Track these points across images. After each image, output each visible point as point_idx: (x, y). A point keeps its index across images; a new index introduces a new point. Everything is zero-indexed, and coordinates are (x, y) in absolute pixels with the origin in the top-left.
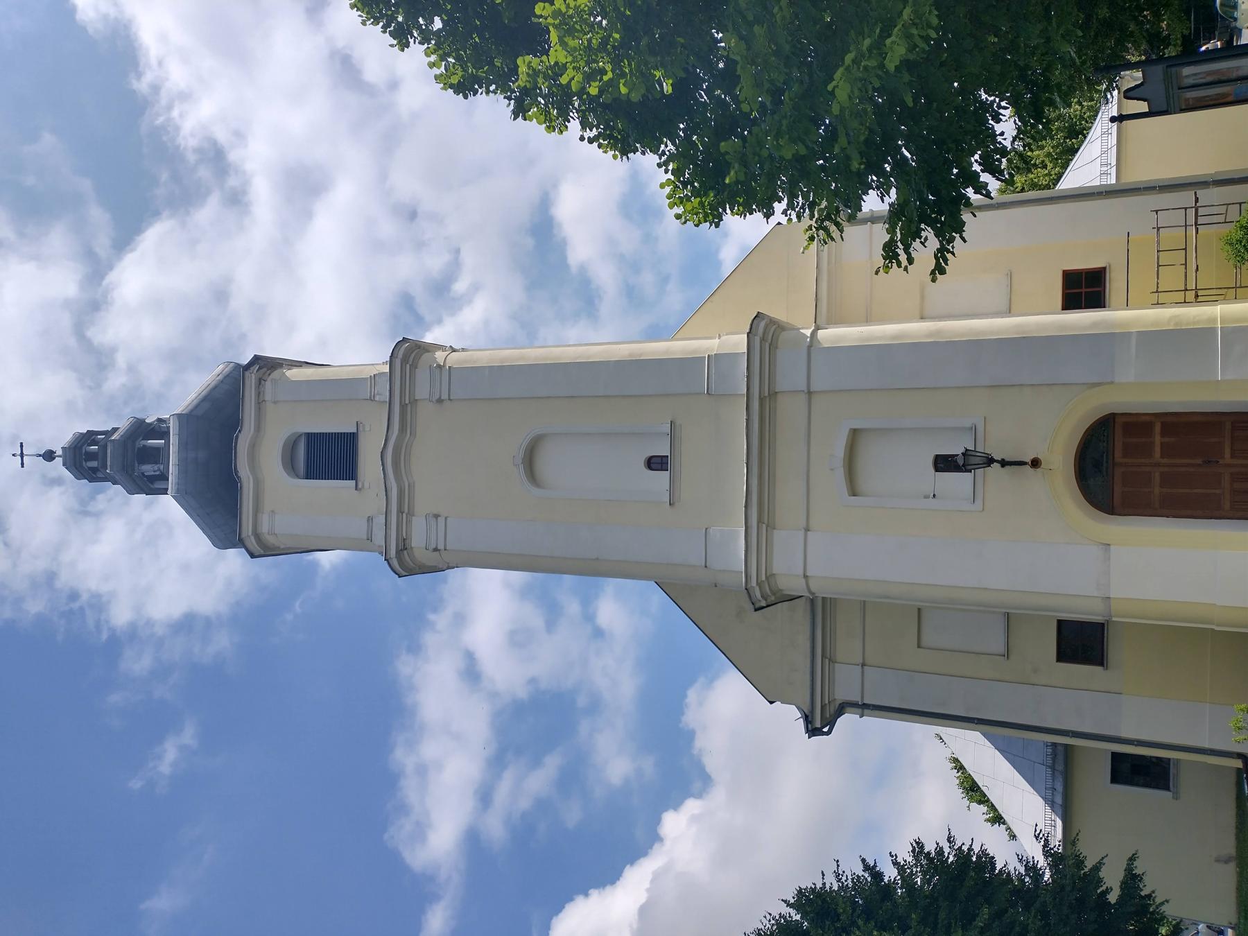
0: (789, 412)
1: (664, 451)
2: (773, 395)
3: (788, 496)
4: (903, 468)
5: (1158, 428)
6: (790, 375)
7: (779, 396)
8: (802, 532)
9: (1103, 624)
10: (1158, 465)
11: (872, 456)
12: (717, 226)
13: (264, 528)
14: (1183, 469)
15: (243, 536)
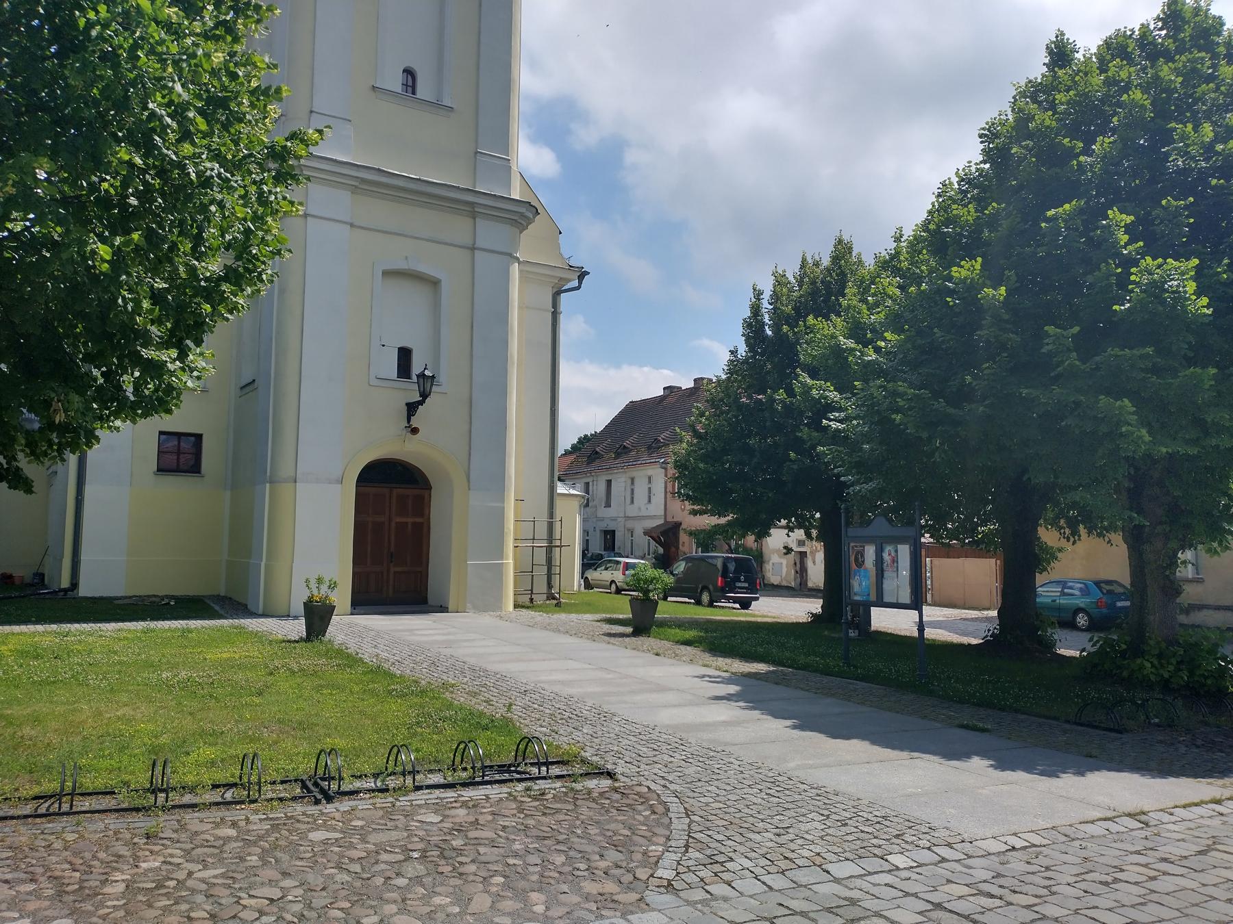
0: (458, 228)
1: (423, 91)
2: (474, 216)
3: (380, 212)
4: (403, 320)
5: (418, 520)
6: (490, 233)
7: (469, 221)
8: (348, 219)
9: (199, 472)
10: (390, 520)
11: (412, 298)
12: (840, 241)
14: (393, 538)
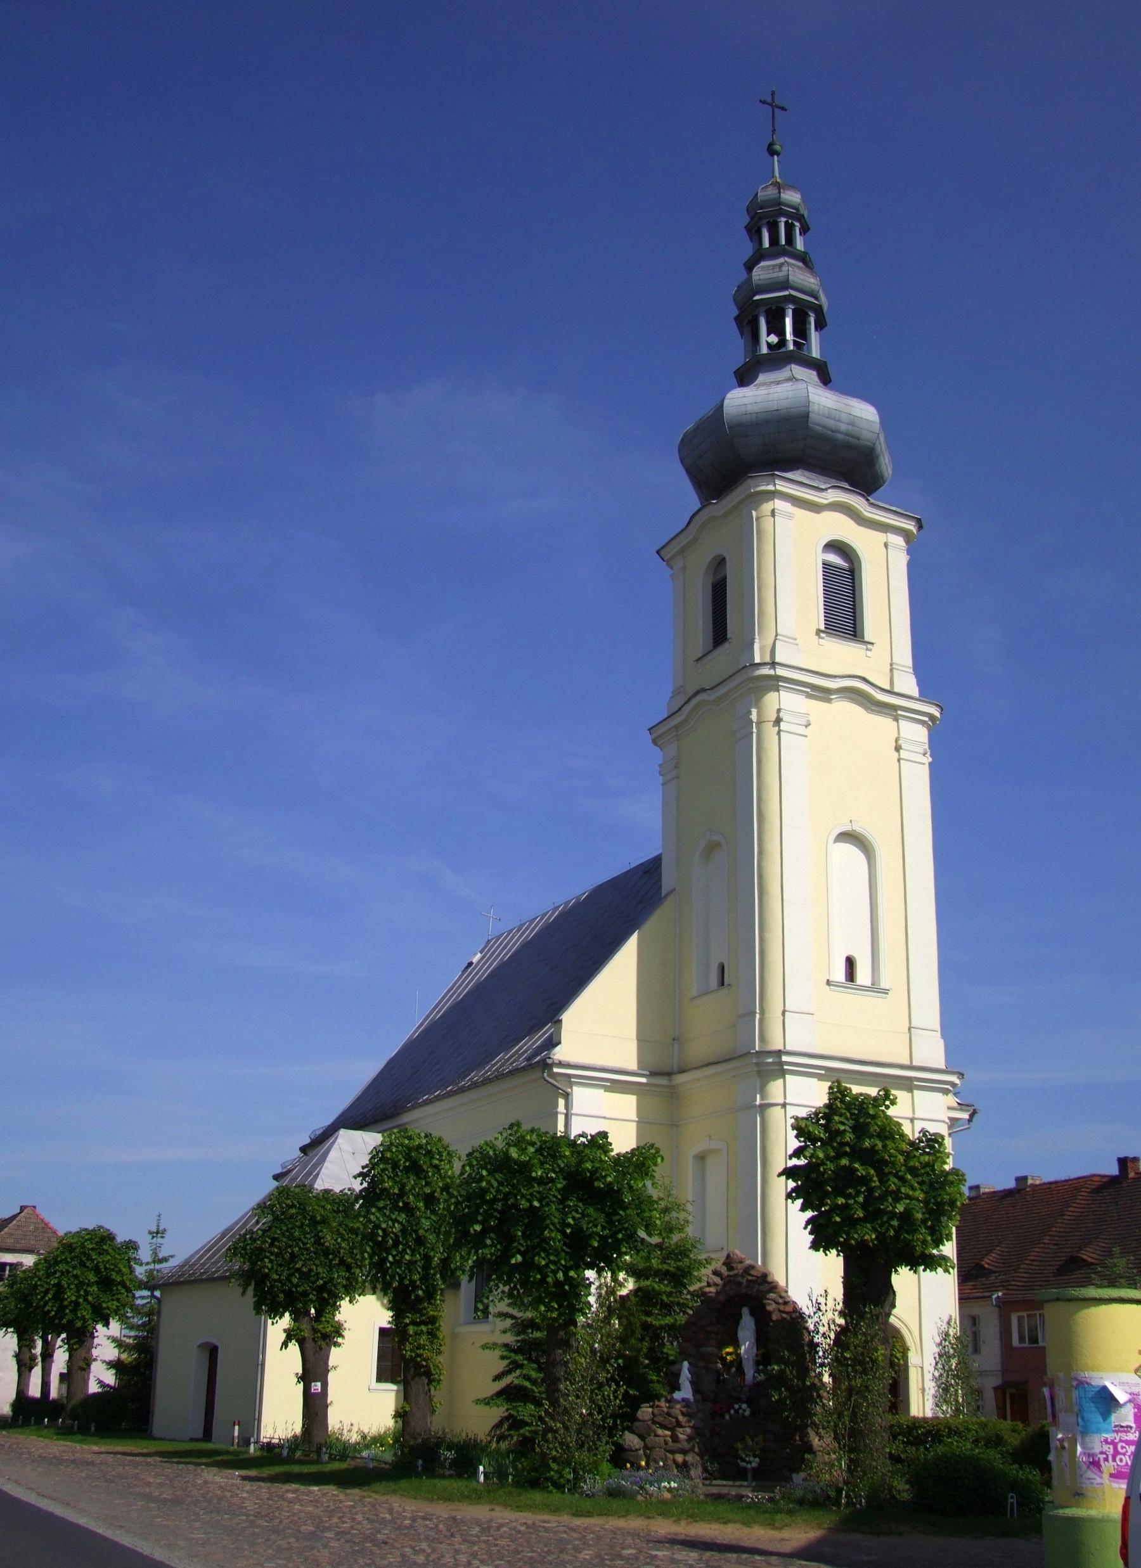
1: (863, 976)
13: (779, 504)
15: (777, 482)
